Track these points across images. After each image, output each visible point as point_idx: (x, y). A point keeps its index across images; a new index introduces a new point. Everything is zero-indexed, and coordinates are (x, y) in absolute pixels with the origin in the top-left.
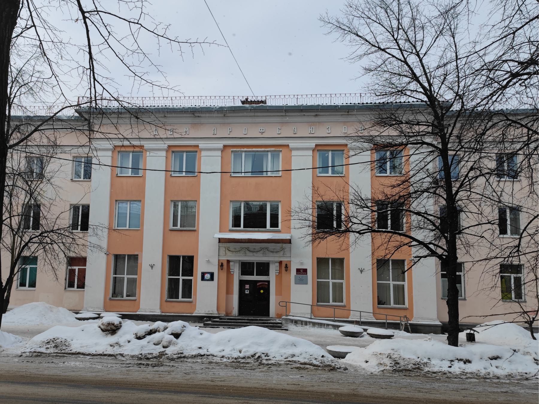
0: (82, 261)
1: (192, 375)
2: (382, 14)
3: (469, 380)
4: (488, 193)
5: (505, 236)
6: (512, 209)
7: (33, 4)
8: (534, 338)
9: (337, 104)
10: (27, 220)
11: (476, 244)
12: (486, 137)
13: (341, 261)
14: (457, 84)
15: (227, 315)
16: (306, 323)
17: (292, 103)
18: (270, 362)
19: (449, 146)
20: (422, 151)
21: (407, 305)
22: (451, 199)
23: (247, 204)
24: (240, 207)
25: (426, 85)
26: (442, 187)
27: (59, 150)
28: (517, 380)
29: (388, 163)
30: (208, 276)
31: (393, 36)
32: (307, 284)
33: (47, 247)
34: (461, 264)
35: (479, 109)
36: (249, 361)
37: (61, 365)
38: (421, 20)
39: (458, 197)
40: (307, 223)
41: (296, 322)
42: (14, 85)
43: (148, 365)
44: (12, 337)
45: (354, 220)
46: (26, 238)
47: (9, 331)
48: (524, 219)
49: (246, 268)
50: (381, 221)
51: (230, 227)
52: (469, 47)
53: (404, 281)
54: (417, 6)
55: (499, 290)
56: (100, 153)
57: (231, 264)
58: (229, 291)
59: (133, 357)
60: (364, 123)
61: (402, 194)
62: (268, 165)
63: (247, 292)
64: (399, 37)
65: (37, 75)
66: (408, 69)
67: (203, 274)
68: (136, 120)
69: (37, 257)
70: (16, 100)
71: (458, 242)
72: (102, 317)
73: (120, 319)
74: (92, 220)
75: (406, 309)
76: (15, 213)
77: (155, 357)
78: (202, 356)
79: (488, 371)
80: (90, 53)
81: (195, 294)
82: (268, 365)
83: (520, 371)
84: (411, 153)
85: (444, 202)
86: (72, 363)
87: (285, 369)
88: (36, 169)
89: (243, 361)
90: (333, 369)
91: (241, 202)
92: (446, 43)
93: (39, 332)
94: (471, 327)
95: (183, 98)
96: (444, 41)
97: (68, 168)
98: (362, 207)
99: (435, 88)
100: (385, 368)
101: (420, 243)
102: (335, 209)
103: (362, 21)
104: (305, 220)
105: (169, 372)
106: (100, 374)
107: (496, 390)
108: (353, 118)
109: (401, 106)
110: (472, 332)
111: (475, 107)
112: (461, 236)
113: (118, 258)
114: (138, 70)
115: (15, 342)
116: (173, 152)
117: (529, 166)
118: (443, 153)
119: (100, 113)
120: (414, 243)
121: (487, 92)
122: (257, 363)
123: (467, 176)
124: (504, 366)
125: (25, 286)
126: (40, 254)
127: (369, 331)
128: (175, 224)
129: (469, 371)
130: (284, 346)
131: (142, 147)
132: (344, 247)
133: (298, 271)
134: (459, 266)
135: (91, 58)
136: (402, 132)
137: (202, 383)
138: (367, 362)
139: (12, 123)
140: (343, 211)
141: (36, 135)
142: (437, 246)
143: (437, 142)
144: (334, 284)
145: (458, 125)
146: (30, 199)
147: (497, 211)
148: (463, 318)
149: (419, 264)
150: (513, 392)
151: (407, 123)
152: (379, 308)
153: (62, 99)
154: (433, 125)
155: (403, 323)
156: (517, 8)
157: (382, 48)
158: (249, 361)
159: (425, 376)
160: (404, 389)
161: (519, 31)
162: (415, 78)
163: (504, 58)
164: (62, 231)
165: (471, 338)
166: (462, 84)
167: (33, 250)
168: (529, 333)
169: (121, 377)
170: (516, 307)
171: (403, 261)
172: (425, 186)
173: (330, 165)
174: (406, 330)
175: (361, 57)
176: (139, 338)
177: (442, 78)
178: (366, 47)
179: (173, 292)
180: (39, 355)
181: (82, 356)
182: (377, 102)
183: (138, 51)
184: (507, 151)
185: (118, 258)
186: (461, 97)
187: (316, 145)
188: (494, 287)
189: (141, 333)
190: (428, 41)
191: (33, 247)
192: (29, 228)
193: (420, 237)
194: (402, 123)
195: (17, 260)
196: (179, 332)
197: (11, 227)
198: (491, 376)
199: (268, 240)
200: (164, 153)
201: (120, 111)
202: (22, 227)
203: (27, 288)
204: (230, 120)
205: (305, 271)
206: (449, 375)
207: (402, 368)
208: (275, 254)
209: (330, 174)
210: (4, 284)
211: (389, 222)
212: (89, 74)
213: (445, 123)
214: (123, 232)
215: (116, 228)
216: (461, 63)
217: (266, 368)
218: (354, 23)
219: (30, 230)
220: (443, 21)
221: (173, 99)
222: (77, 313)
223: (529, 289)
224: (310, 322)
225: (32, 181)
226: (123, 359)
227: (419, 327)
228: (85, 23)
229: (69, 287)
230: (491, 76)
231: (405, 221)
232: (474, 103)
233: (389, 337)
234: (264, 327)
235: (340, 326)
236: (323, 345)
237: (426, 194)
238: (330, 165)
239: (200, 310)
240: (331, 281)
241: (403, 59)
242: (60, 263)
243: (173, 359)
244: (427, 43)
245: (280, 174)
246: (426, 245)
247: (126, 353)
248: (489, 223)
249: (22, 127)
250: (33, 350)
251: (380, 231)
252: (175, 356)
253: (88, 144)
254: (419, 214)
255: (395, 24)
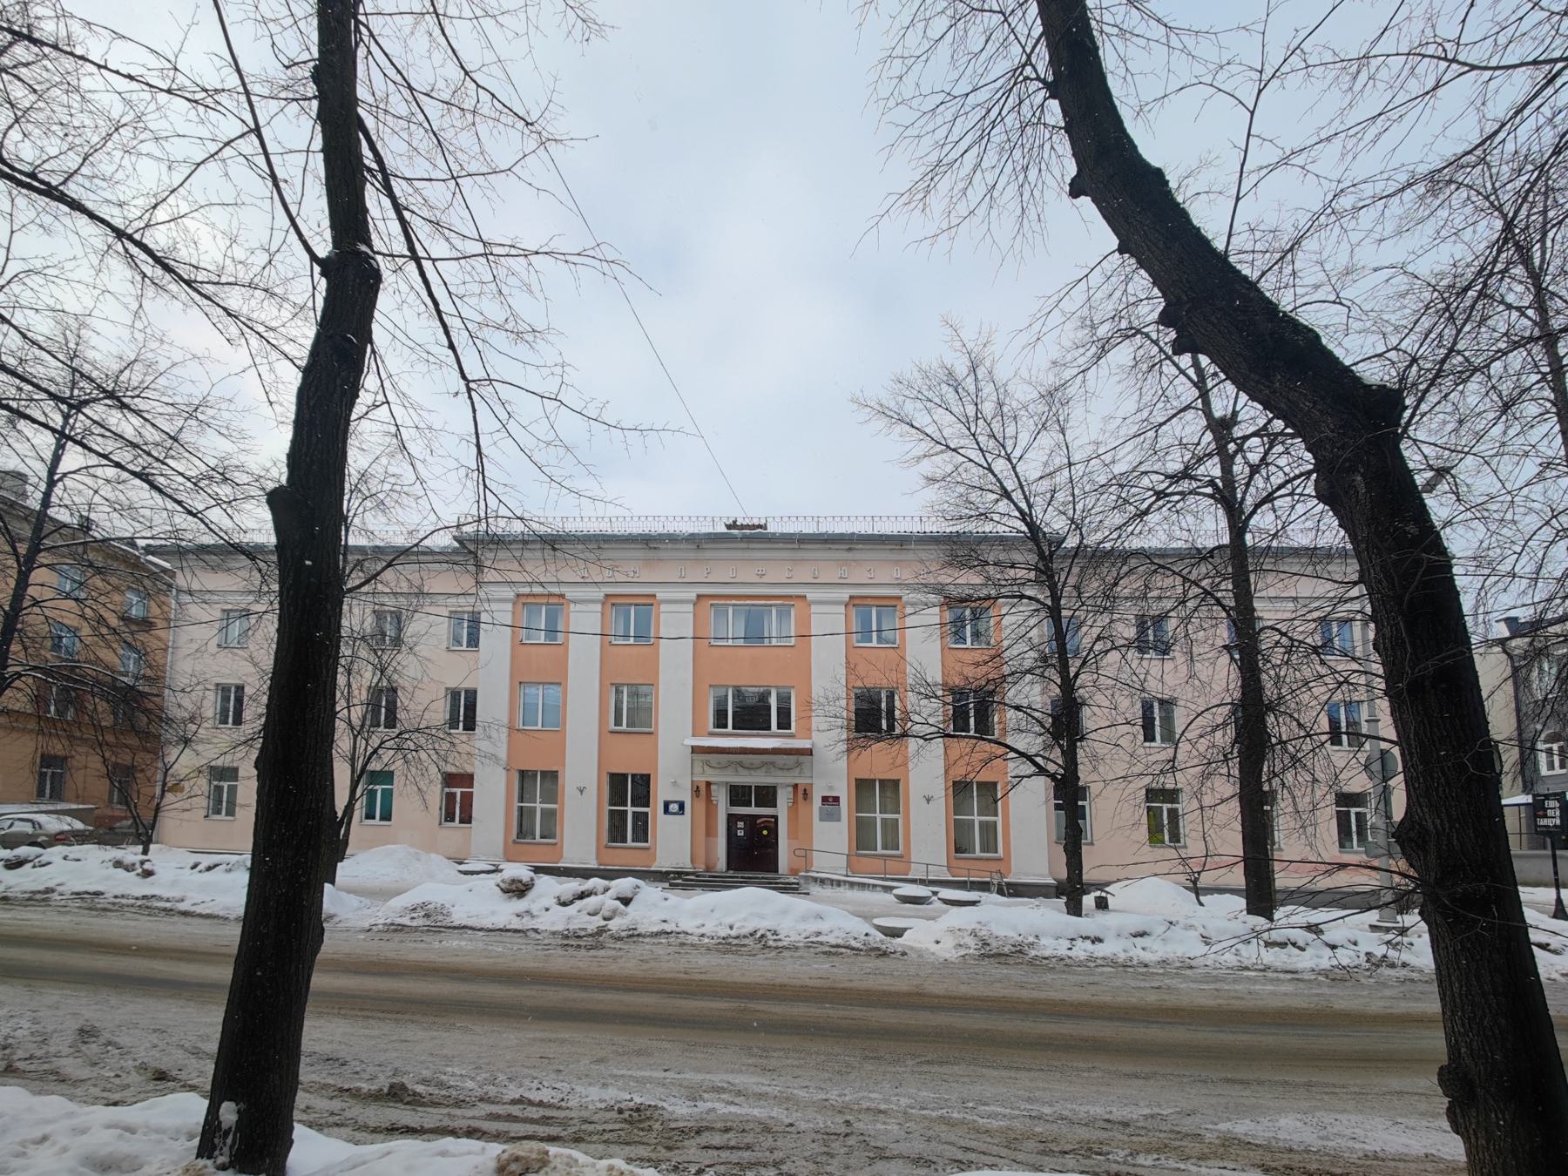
0: (467, 779)
1: (652, 964)
2: (951, 395)
3: (1099, 970)
4: (1124, 676)
5: (1153, 744)
6: (1162, 702)
7: (385, 367)
8: (1201, 904)
9: (883, 532)
10: (376, 713)
11: (1109, 756)
12: (1119, 589)
13: (896, 783)
14: (1071, 506)
15: (708, 869)
16: (839, 883)
17: (809, 528)
18: (780, 944)
19: (1063, 602)
20: (1021, 609)
21: (1001, 853)
22: (1068, 685)
23: (738, 693)
24: (727, 696)
25: (1023, 505)
26: (1054, 666)
27: (428, 601)
28: (1178, 968)
29: (968, 627)
30: (674, 807)
31: (969, 429)
32: (839, 820)
33: (409, 756)
34: (1084, 789)
35: (1108, 545)
36: (746, 941)
37: (436, 945)
38: (1011, 405)
39: (1079, 682)
40: (840, 722)
41: (823, 881)
42: (354, 496)
43: (579, 946)
44: (354, 900)
45: (916, 718)
46: (375, 742)
47: (349, 891)
48: (1180, 719)
49: (739, 795)
50: (959, 718)
51: (711, 728)
52: (1089, 450)
53: (996, 815)
54: (1005, 385)
55: (1144, 828)
56: (494, 606)
57: (713, 787)
58: (710, 831)
59: (554, 933)
60: (928, 563)
61: (991, 677)
62: (772, 626)
63: (740, 833)
64: (979, 430)
65: (392, 480)
66: (994, 480)
67: (666, 805)
68: (552, 552)
69: (392, 772)
70: (356, 521)
71: (1080, 753)
72: (501, 871)
73: (532, 874)
74: (481, 714)
75: (999, 859)
76: (356, 701)
77: (590, 935)
78: (668, 933)
79: (1131, 954)
80: (478, 446)
81: (655, 836)
82: (777, 948)
83: (1179, 954)
84: (1003, 612)
85: (1058, 691)
86: (454, 942)
87: (806, 955)
88: (390, 631)
89: (735, 942)
90: (885, 954)
91: (727, 687)
92: (1053, 443)
93: (398, 893)
94: (1100, 886)
95: (628, 519)
96: (1048, 439)
97: (443, 628)
98: (927, 697)
99: (1038, 512)
100: (967, 951)
101: (1022, 754)
102: (884, 699)
103: (919, 405)
104: (836, 717)
105: (615, 959)
106: (501, 960)
107: (1143, 984)
108: (910, 556)
109: (985, 539)
110: (1104, 894)
111: (1102, 542)
112: (1084, 743)
113: (525, 776)
114: (556, 473)
115: (359, 909)
116: (613, 605)
117: (1187, 635)
118: (1054, 612)
119: (492, 542)
120: (1012, 755)
121: (1118, 519)
122: (759, 946)
123: (1091, 649)
124: (1155, 948)
125: (374, 818)
126: (398, 766)
127: (940, 895)
128: (618, 722)
129: (1100, 954)
130: (804, 919)
131: (562, 596)
132: (899, 760)
133: (825, 799)
134: (1082, 792)
135: (479, 452)
136: (988, 578)
137: (670, 975)
138: (938, 942)
139: (350, 558)
140: (897, 703)
141: (388, 575)
142: (1048, 759)
143: (1043, 595)
144: (883, 820)
145: (1076, 570)
146: (380, 679)
147: (1139, 705)
148: (1088, 875)
149: (1019, 788)
150: (1169, 988)
151: (995, 564)
152: (957, 858)
153: (432, 517)
154: (1036, 569)
155: (995, 882)
156: (1160, 392)
157: (952, 446)
158: (746, 941)
159: (1030, 963)
160: (999, 985)
161: (1164, 427)
162: (1006, 494)
163: (1142, 468)
164: (434, 732)
165: (1102, 904)
166: (1079, 506)
167: (386, 761)
168: (1193, 895)
169: (536, 965)
170: (1172, 853)
171: (995, 784)
172: (1028, 664)
173: (874, 628)
174: (1000, 892)
175: (919, 459)
176: (564, 904)
177: (1049, 495)
178: (926, 445)
179: (616, 831)
180: (401, 928)
181: (470, 932)
182: (948, 530)
183: (557, 442)
184: (1152, 613)
185: (525, 776)
186: (1078, 527)
187: (851, 597)
188: (1136, 824)
189: (566, 897)
190: (1024, 438)
191: (387, 755)
192: (379, 726)
193: (1021, 747)
194: (988, 564)
195: (360, 777)
196: (630, 896)
197: (350, 723)
198: (1135, 963)
199: (773, 749)
200: (598, 607)
201: (526, 538)
202: (368, 723)
203: (377, 821)
204: (708, 554)
205: (836, 799)
206: (1068, 961)
207: (995, 951)
208: (785, 773)
209: (874, 644)
210: (340, 815)
211: (972, 721)
212: (475, 478)
213: (1055, 566)
214: (532, 734)
215: (521, 727)
216: (1078, 470)
217: (773, 954)
218: (905, 408)
219: (382, 729)
220: (1047, 408)
221: (614, 519)
222: (460, 863)
223: (1191, 826)
224: (845, 882)
225: (383, 650)
226: (538, 937)
227: (1020, 888)
228: (470, 397)
229: (446, 820)
230: (1123, 495)
231: (996, 719)
232: (1099, 536)
233: (973, 903)
234: (774, 889)
235: (892, 888)
236: (867, 917)
237: (1029, 677)
238: (874, 628)
239: (663, 863)
240: (879, 816)
241: (985, 465)
242: (431, 782)
243: (620, 939)
244: (1022, 443)
245: (793, 641)
246: (1030, 758)
247: (541, 927)
248: (1128, 723)
249: (366, 564)
250: (389, 921)
251: (957, 736)
252: (624, 934)
253: (473, 591)
254: (1018, 708)
255: (971, 410)
